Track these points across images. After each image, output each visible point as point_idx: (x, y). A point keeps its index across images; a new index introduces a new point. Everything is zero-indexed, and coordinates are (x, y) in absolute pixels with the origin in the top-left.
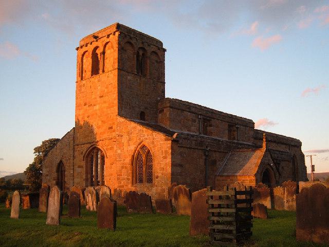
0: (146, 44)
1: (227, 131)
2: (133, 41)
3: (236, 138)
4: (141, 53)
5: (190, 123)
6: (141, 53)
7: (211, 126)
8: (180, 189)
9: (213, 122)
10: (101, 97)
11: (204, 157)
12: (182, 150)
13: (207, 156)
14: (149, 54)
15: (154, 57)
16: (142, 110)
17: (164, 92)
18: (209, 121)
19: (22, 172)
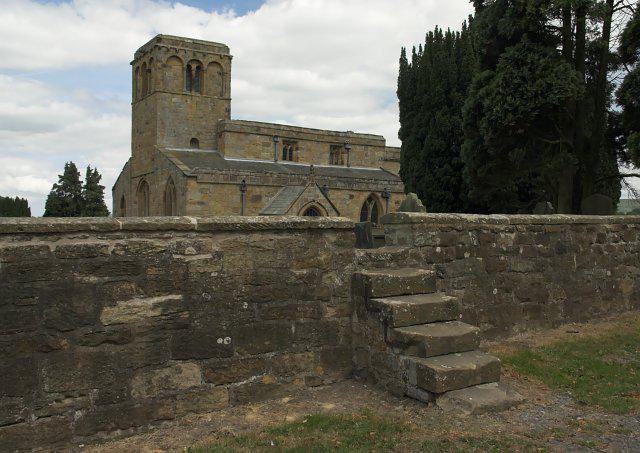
0: (198, 55)
1: (328, 155)
2: (180, 55)
3: (345, 162)
4: (194, 66)
5: (259, 148)
6: (194, 66)
7: (297, 149)
8: (623, 353)
9: (300, 144)
10: (147, 123)
11: (240, 193)
12: (203, 186)
13: (243, 191)
14: (205, 66)
15: (215, 69)
16: (193, 136)
17: (228, 111)
18: (296, 142)
19: (456, 28)
